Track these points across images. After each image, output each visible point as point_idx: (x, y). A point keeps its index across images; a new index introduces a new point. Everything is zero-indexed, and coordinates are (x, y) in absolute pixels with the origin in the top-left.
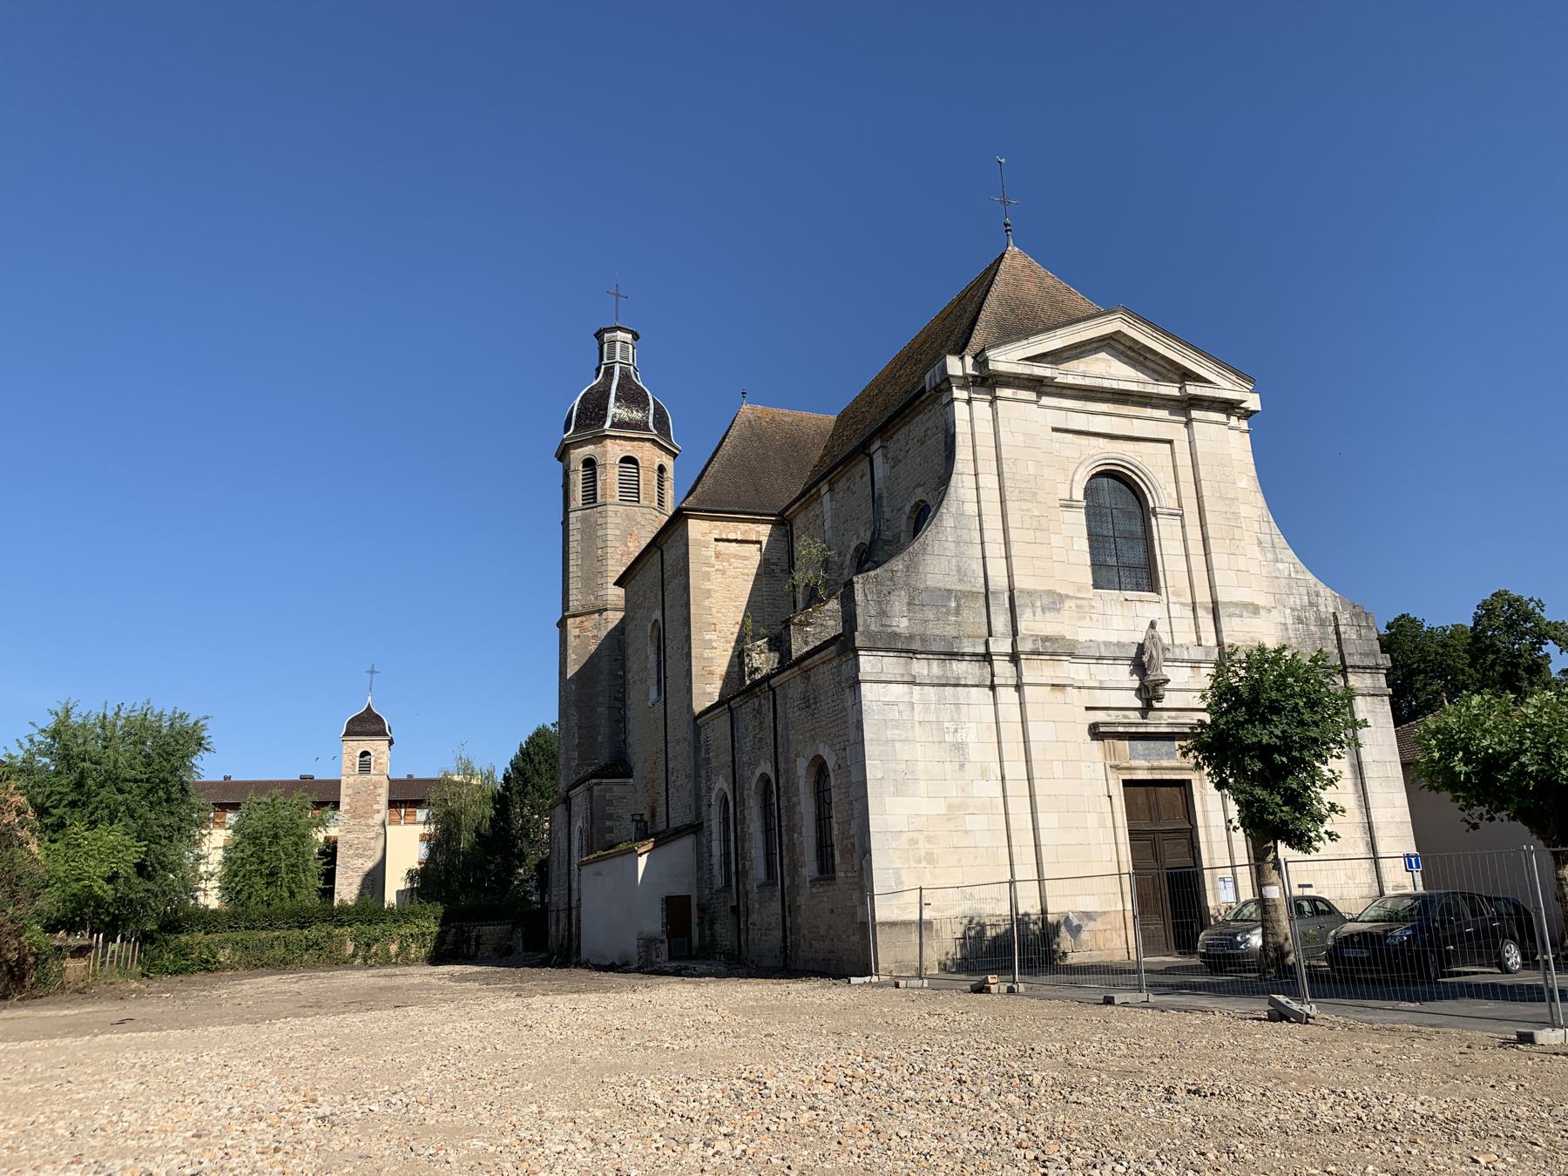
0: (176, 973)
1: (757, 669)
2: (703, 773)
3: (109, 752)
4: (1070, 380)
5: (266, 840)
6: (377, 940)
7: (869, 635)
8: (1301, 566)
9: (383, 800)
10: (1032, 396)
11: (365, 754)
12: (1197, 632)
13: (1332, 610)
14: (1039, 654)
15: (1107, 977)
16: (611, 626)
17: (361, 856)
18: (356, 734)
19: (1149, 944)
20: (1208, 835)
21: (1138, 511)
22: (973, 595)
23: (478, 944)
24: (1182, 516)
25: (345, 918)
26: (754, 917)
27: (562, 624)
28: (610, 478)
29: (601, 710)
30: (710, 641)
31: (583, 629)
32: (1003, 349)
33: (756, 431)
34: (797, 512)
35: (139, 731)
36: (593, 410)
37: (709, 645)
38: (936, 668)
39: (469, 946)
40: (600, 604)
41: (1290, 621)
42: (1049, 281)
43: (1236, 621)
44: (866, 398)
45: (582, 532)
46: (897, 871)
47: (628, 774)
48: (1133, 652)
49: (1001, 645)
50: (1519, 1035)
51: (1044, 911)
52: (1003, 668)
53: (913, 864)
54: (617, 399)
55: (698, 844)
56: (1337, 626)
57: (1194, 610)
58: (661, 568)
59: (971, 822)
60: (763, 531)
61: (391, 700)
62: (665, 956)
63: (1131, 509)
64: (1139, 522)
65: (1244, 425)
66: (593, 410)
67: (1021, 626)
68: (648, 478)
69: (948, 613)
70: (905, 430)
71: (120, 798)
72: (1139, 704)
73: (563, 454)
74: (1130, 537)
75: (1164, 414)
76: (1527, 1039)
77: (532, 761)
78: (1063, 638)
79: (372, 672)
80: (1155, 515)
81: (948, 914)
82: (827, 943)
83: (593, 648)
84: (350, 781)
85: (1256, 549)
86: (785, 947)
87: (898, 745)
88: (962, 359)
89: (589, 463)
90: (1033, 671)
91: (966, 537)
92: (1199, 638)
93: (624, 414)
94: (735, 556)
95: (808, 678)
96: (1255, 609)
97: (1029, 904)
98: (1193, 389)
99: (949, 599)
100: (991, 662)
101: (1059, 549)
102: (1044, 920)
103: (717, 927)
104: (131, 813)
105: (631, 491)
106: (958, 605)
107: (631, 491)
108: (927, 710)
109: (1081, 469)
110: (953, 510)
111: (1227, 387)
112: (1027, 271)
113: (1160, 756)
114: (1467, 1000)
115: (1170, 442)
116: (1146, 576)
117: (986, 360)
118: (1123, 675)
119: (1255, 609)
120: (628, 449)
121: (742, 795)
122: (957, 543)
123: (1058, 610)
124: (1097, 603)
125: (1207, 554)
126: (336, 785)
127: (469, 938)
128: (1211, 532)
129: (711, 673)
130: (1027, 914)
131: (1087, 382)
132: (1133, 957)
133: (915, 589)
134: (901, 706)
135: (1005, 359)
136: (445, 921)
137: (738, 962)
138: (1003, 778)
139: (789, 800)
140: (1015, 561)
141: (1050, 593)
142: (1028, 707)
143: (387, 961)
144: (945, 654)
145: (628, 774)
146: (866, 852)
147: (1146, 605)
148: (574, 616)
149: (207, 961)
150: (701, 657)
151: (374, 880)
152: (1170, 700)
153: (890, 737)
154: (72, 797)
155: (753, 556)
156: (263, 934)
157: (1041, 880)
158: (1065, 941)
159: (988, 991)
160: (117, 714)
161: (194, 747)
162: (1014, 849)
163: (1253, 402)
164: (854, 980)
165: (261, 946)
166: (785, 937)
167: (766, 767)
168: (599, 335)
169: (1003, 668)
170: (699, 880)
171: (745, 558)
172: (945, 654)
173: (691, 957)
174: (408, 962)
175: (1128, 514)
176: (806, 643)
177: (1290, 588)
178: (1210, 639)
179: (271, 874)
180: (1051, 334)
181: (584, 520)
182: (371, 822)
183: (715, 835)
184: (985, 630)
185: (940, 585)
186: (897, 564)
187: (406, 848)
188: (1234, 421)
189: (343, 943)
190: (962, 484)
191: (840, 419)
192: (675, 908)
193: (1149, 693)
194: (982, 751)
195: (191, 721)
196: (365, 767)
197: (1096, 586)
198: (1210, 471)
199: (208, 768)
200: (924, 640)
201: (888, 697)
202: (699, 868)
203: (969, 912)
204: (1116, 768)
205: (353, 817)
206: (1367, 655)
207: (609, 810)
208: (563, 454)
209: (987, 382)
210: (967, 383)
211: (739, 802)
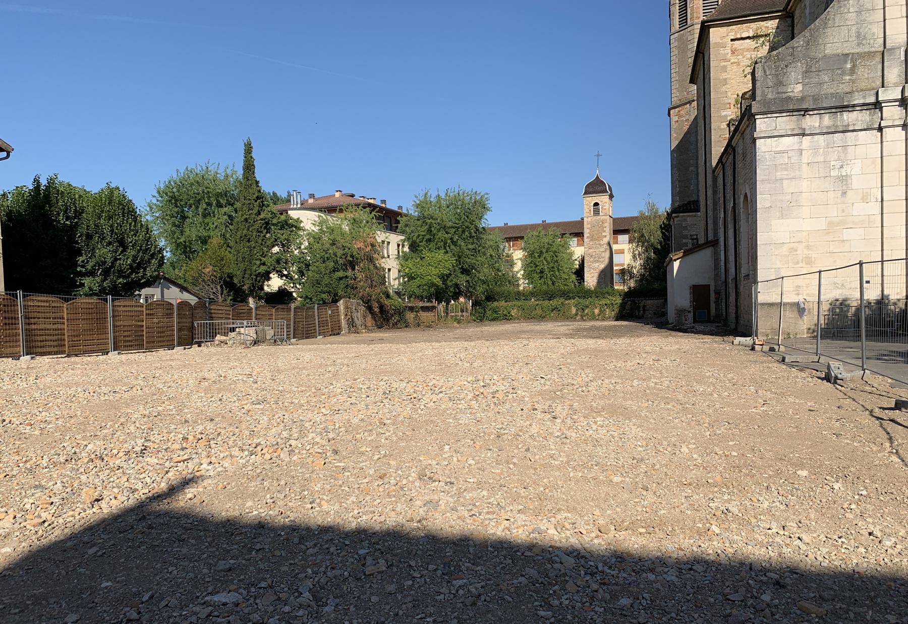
0: (494, 320)
5: (536, 255)
7: (765, 102)
11: (596, 204)
17: (597, 261)
22: (870, 55)
23: (644, 310)
27: (669, 114)
35: (454, 203)
38: (827, 120)
39: (639, 311)
40: (690, 97)
45: (678, 48)
47: (697, 210)
53: (791, 265)
59: (846, 234)
60: (771, 25)
69: (844, 73)
79: (598, 155)
83: (686, 128)
87: (785, 182)
99: (846, 62)
100: (881, 109)
106: (854, 66)
122: (859, 13)
134: (791, 154)
143: (593, 318)
148: (674, 108)
151: (606, 275)
154: (428, 237)
174: (604, 319)
179: (542, 272)
181: (679, 39)
182: (602, 242)
184: (879, 83)
185: (839, 51)
192: (699, 293)
196: (596, 212)
199: (492, 220)
202: (716, 266)
205: (592, 240)
207: (685, 232)
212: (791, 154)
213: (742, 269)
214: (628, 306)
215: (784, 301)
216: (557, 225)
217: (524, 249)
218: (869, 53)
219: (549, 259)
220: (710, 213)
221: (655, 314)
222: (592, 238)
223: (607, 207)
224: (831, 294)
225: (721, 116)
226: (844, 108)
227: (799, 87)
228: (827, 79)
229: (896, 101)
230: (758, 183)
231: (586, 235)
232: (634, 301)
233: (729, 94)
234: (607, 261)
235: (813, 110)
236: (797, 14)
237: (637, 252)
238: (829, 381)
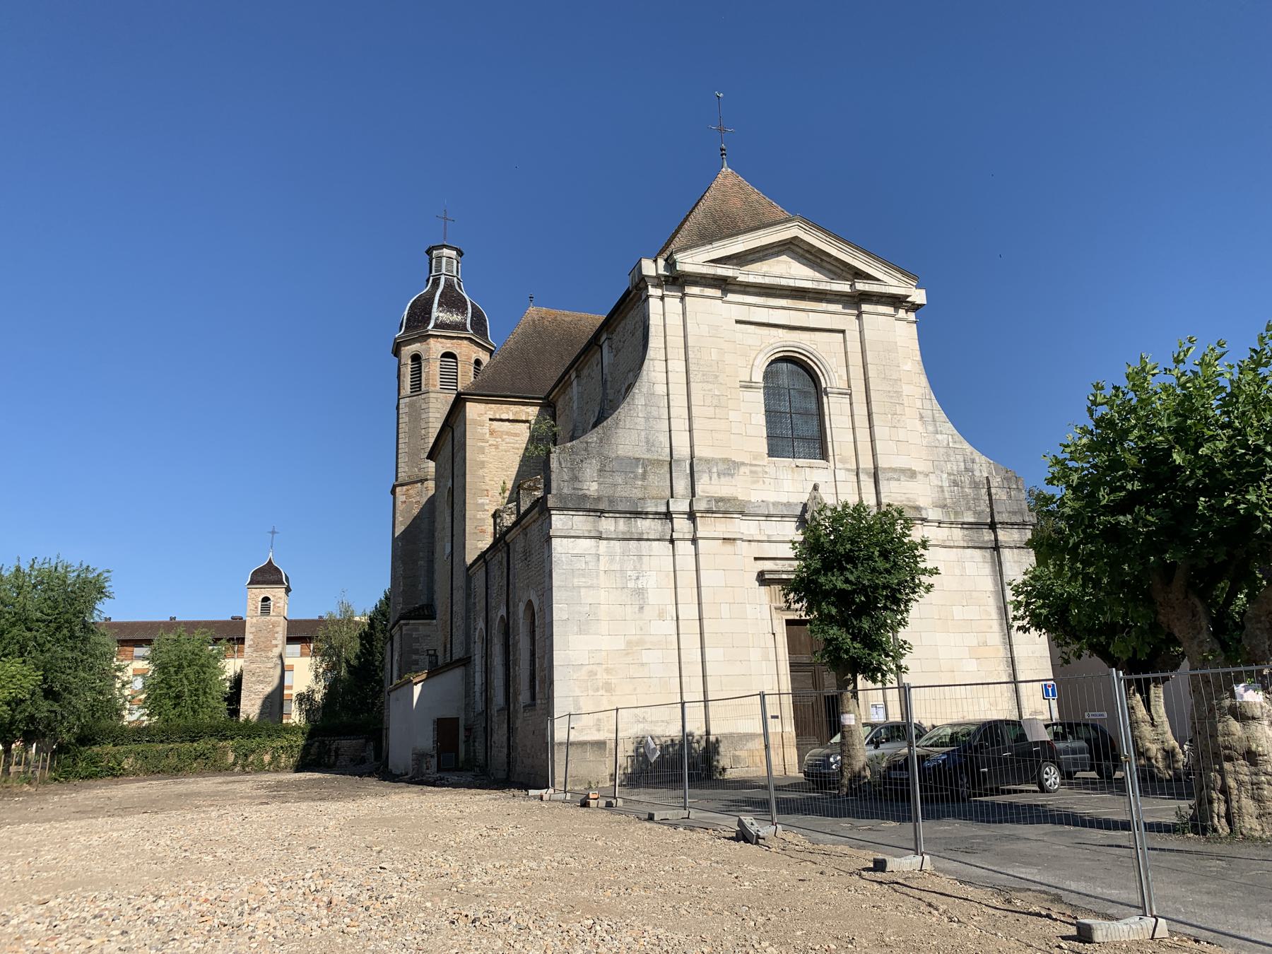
0: (89, 777)
3: (21, 598)
4: (751, 279)
5: (172, 670)
6: (253, 752)
7: (561, 497)
10: (718, 293)
11: (266, 599)
12: (860, 494)
13: (985, 475)
17: (261, 682)
18: (258, 583)
21: (813, 390)
22: (659, 462)
23: (337, 756)
25: (228, 733)
27: (393, 492)
28: (433, 370)
29: (421, 563)
30: (483, 504)
31: (408, 496)
32: (689, 252)
33: (538, 329)
36: (420, 313)
38: (622, 525)
39: (329, 757)
40: (422, 475)
41: (946, 484)
42: (754, 197)
43: (893, 484)
45: (409, 415)
46: (576, 700)
47: (432, 616)
48: (798, 511)
50: (876, 862)
51: (708, 733)
52: (682, 524)
53: (591, 693)
54: (440, 305)
56: (989, 488)
57: (857, 475)
58: (450, 445)
59: (646, 657)
60: (532, 412)
63: (807, 389)
64: (814, 400)
65: (912, 316)
66: (420, 313)
69: (636, 478)
70: (622, 324)
71: (28, 634)
73: (397, 352)
75: (838, 308)
76: (880, 866)
78: (735, 499)
79: (273, 532)
80: (827, 394)
83: (416, 512)
84: (253, 621)
85: (918, 423)
87: (583, 590)
88: (655, 261)
89: (416, 358)
91: (655, 414)
93: (446, 317)
94: (508, 433)
97: (696, 726)
98: (861, 286)
102: (707, 740)
104: (40, 647)
106: (645, 472)
108: (612, 561)
109: (761, 356)
110: (644, 390)
111: (893, 284)
112: (736, 188)
114: (951, 820)
115: (843, 332)
116: (819, 447)
117: (675, 262)
119: (912, 474)
120: (448, 346)
122: (647, 419)
123: (732, 475)
124: (771, 470)
125: (871, 427)
128: (874, 409)
129: (483, 531)
130: (691, 734)
131: (767, 281)
133: (607, 458)
134: (588, 558)
140: (695, 433)
143: (261, 769)
144: (630, 513)
145: (432, 616)
146: (552, 683)
147: (815, 471)
148: (402, 485)
150: (475, 518)
151: (274, 703)
153: (576, 584)
155: (523, 432)
156: (161, 746)
158: (724, 760)
160: (32, 566)
161: (94, 594)
162: (684, 679)
163: (919, 296)
165: (159, 756)
167: (503, 612)
169: (682, 524)
170: (467, 705)
171: (516, 435)
172: (630, 513)
173: (457, 769)
175: (805, 394)
177: (948, 455)
179: (178, 697)
180: (734, 239)
181: (411, 405)
182: (270, 654)
183: (478, 668)
184: (668, 493)
185: (630, 454)
186: (593, 437)
187: (304, 674)
188: (902, 313)
189: (225, 753)
190: (653, 369)
192: (445, 728)
194: (660, 596)
197: (772, 453)
198: (880, 357)
199: (110, 610)
200: (611, 501)
202: (468, 692)
203: (640, 734)
206: (1014, 513)
207: (416, 646)
209: (677, 281)
210: (661, 282)
212: (588, 558)
213: (521, 698)
215: (572, 739)
216: (209, 625)
217: (152, 660)
218: (659, 461)
219: (192, 677)
220: (459, 622)
221: (352, 760)
222: (257, 648)
223: (281, 604)
224: (631, 729)
225: (478, 504)
227: (594, 486)
228: (620, 481)
229: (684, 513)
230: (554, 589)
231: (247, 642)
232: (323, 742)
233: (487, 479)
234: (276, 682)
235: (609, 512)
236: (560, 405)
237: (321, 670)
238: (747, 841)
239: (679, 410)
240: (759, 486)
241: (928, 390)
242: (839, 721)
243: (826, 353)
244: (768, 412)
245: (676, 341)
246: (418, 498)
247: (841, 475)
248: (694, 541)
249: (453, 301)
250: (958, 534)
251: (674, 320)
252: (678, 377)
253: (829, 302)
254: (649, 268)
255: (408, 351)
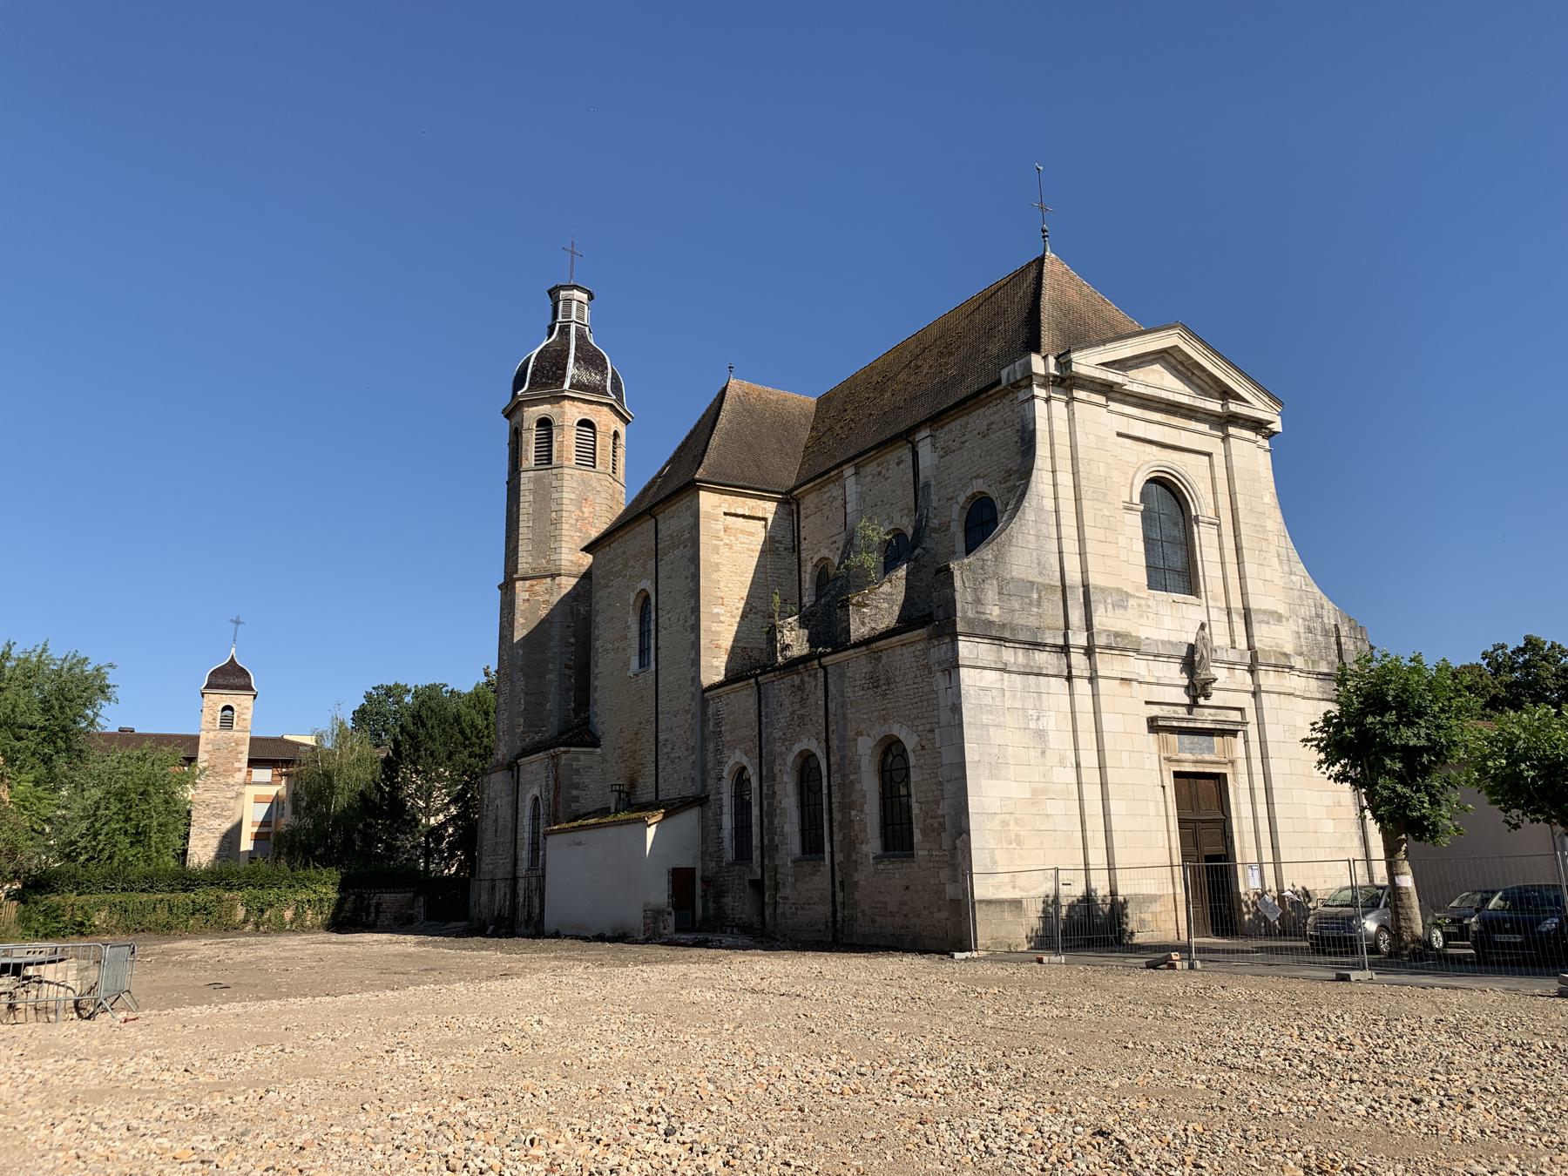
1: (788, 646)
2: (711, 746)
4: (1135, 388)
7: (970, 622)
8: (1310, 580)
9: (245, 758)
12: (1231, 636)
14: (1112, 648)
15: (1159, 957)
16: (564, 592)
18: (218, 687)
19: (1194, 925)
20: (1239, 825)
23: (378, 912)
24: (1219, 526)
26: (787, 891)
28: (567, 441)
30: (718, 615)
34: (809, 492)
37: (716, 618)
39: (368, 915)
40: (553, 570)
41: (1302, 630)
44: (876, 379)
45: (535, 493)
47: (595, 743)
48: (1184, 652)
49: (1079, 639)
51: (1113, 893)
52: (1078, 660)
54: (577, 360)
55: (703, 818)
56: (1338, 637)
57: (1229, 614)
60: (769, 509)
61: (255, 660)
62: (671, 929)
65: (1266, 443)
67: (1096, 621)
68: (603, 442)
69: (1030, 604)
72: (1187, 701)
73: (513, 411)
74: (1174, 542)
75: (1204, 427)
77: (424, 725)
81: (1033, 893)
82: (934, 922)
83: (543, 613)
84: (209, 737)
86: (835, 922)
89: (545, 423)
90: (1108, 665)
92: (1233, 642)
94: (742, 531)
95: (879, 659)
96: (1279, 618)
98: (1234, 407)
101: (1120, 553)
103: (728, 900)
105: (588, 456)
107: (588, 456)
111: (1260, 408)
113: (1202, 751)
115: (1209, 455)
118: (1174, 673)
119: (1279, 618)
120: (586, 412)
121: (771, 770)
122: (1038, 537)
126: (195, 740)
127: (369, 905)
132: (1184, 937)
135: (1086, 362)
136: (343, 887)
137: (767, 934)
138: (1078, 765)
139: (844, 777)
141: (1118, 590)
142: (1102, 699)
143: (281, 929)
145: (595, 743)
146: (962, 830)
149: (82, 924)
150: (709, 630)
152: (1216, 698)
155: (756, 535)
156: (145, 897)
157: (1087, 870)
159: (1172, 966)
162: (1089, 834)
163: (1277, 427)
164: (958, 955)
165: (143, 910)
166: (834, 912)
168: (553, 293)
169: (1078, 660)
171: (751, 534)
176: (863, 624)
178: (1242, 643)
180: (1123, 342)
181: (537, 481)
182: (231, 781)
185: (1023, 576)
189: (233, 907)
191: (824, 402)
192: (681, 879)
193: (1198, 689)
194: (1060, 740)
195: (89, 669)
196: (227, 723)
198: (1237, 479)
200: (1013, 629)
201: (985, 682)
202: (704, 840)
204: (1168, 759)
207: (576, 779)
208: (513, 411)
209: (1066, 382)
211: (767, 777)
214: (348, 906)
221: (396, 919)
226: (1037, 645)
232: (360, 896)
233: (722, 585)
239: (1069, 531)
240: (1143, 621)
241: (1282, 526)
242: (206, 872)
243: (1194, 474)
244: (1147, 540)
245: (1063, 450)
246: (547, 597)
247: (1214, 614)
248: (1092, 679)
249: (591, 359)
250: (1313, 684)
251: (1061, 427)
252: (1066, 492)
253: (1198, 420)
254: (1038, 364)
255: (532, 414)
